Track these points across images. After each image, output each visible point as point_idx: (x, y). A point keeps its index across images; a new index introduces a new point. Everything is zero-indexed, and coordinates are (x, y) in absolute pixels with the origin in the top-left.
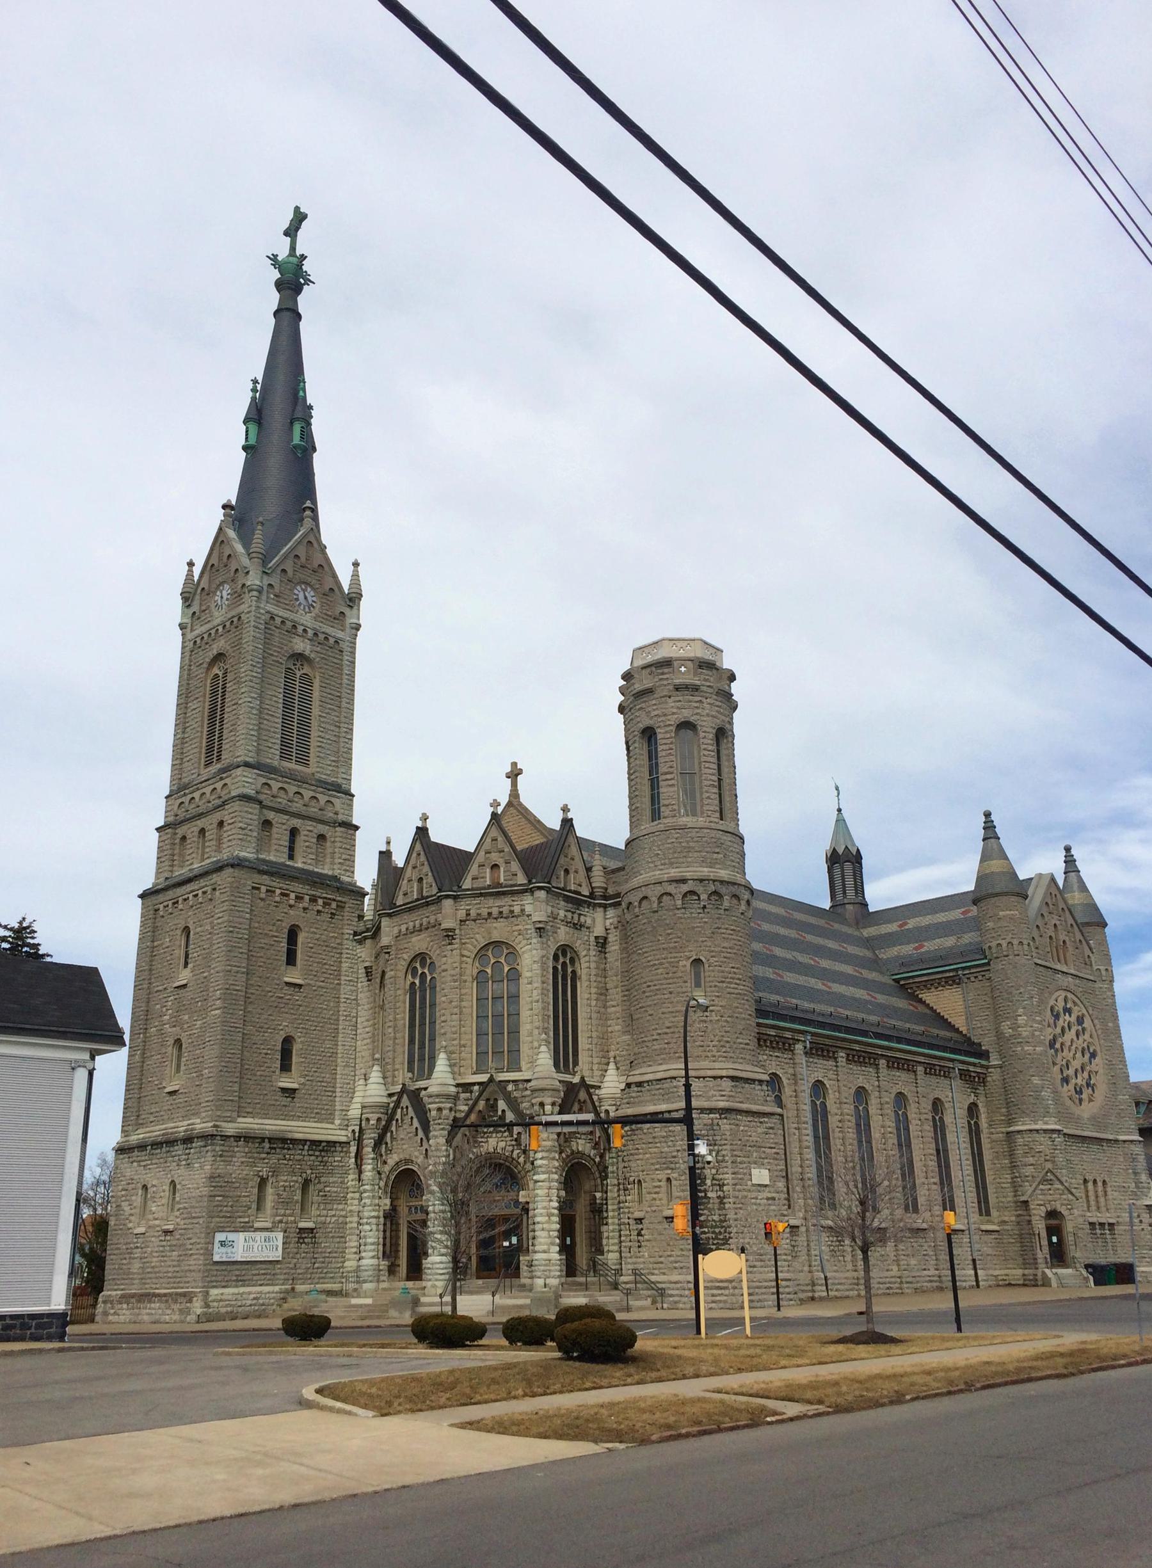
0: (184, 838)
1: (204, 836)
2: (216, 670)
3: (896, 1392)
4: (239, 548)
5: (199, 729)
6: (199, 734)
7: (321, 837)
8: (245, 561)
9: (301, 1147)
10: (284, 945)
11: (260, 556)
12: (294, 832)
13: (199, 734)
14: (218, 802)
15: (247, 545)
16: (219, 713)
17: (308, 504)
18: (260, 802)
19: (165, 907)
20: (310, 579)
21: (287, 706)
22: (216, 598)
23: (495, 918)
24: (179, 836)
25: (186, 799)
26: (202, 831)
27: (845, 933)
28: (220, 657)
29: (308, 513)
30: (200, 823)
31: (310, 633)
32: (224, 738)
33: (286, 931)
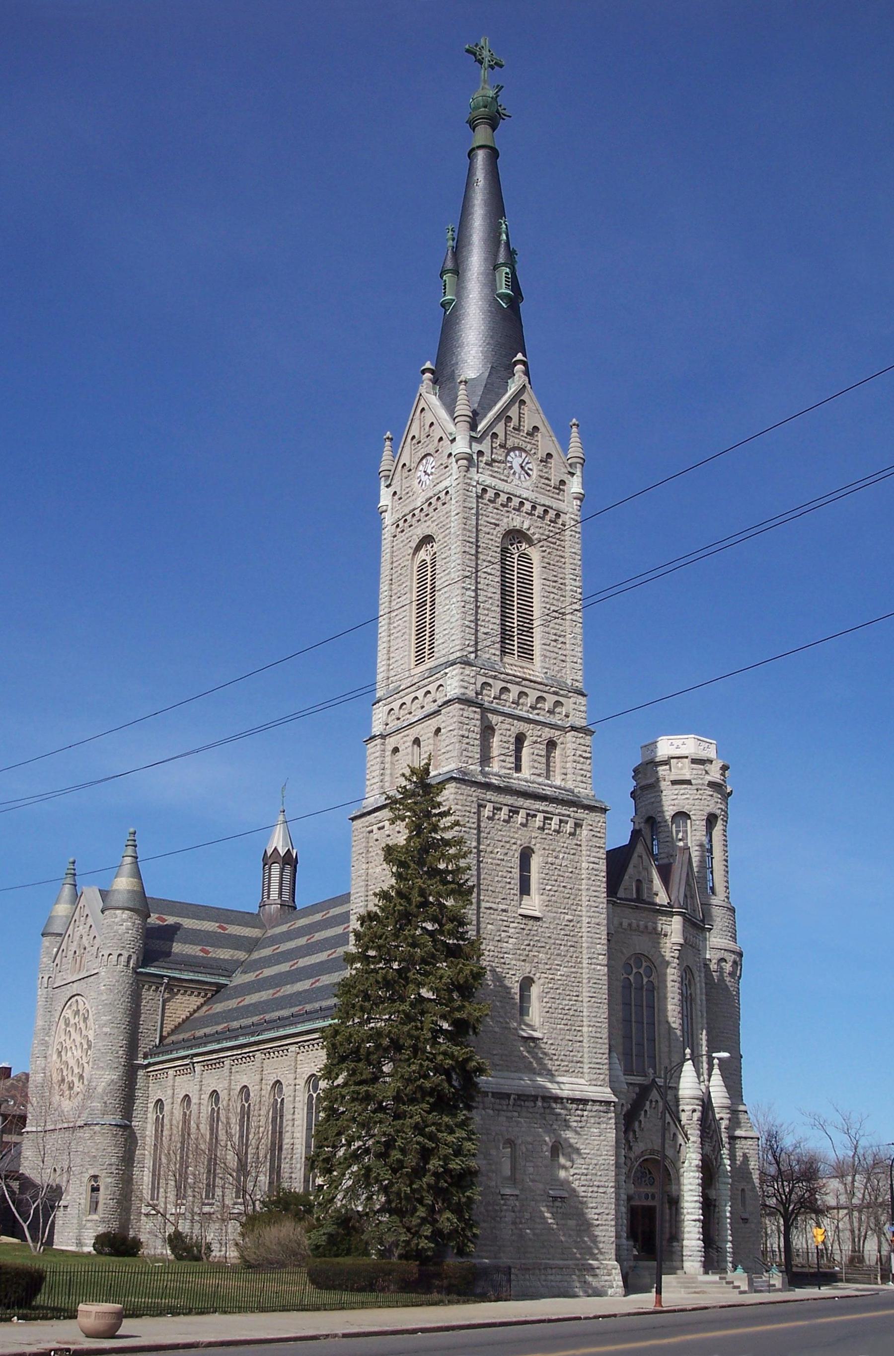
0: (396, 750)
1: (419, 746)
2: (422, 554)
3: (314, 1245)
4: (443, 414)
5: (408, 583)
6: (407, 642)
7: (551, 745)
8: (451, 427)
9: (532, 1104)
10: (517, 870)
11: (468, 419)
12: (520, 739)
13: (407, 642)
14: (434, 707)
15: (451, 410)
16: (428, 626)
17: (520, 356)
18: (480, 706)
19: (379, 829)
20: (524, 445)
21: (505, 593)
22: (419, 474)
23: (650, 933)
24: (390, 748)
25: (396, 705)
26: (417, 742)
27: (707, 1046)
28: (428, 539)
29: (519, 367)
30: (413, 733)
31: (528, 506)
32: (436, 631)
33: (517, 855)
